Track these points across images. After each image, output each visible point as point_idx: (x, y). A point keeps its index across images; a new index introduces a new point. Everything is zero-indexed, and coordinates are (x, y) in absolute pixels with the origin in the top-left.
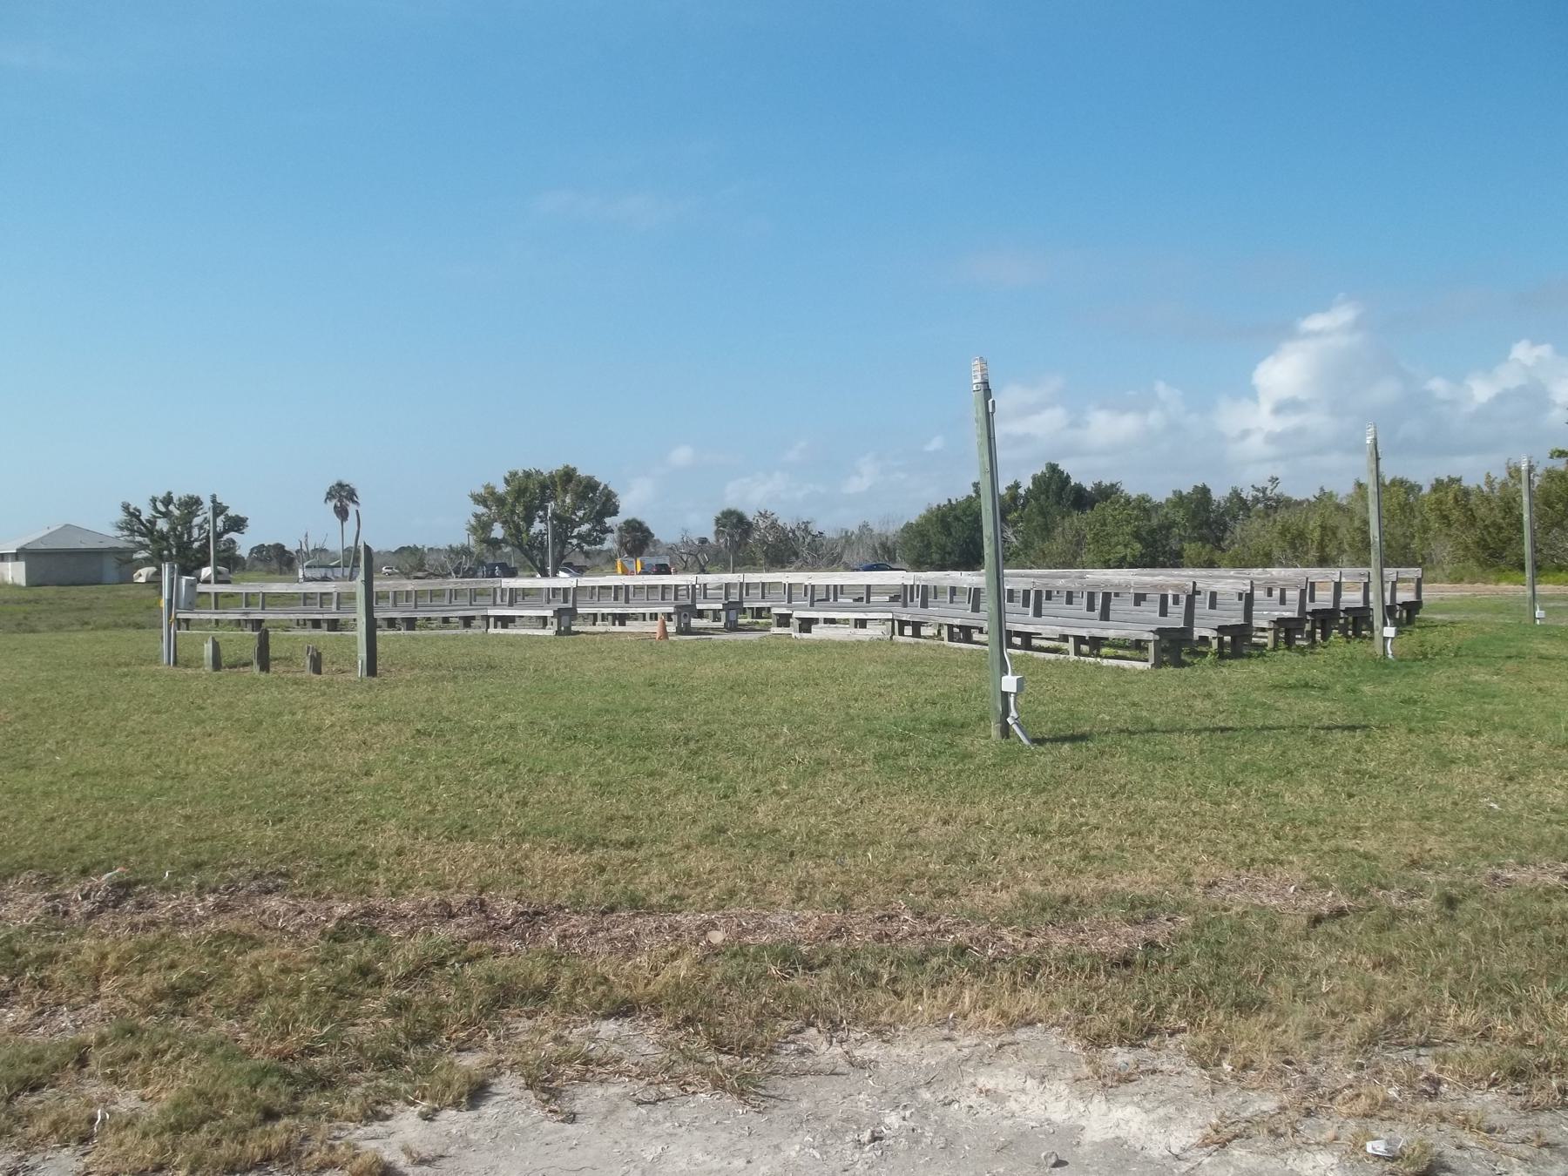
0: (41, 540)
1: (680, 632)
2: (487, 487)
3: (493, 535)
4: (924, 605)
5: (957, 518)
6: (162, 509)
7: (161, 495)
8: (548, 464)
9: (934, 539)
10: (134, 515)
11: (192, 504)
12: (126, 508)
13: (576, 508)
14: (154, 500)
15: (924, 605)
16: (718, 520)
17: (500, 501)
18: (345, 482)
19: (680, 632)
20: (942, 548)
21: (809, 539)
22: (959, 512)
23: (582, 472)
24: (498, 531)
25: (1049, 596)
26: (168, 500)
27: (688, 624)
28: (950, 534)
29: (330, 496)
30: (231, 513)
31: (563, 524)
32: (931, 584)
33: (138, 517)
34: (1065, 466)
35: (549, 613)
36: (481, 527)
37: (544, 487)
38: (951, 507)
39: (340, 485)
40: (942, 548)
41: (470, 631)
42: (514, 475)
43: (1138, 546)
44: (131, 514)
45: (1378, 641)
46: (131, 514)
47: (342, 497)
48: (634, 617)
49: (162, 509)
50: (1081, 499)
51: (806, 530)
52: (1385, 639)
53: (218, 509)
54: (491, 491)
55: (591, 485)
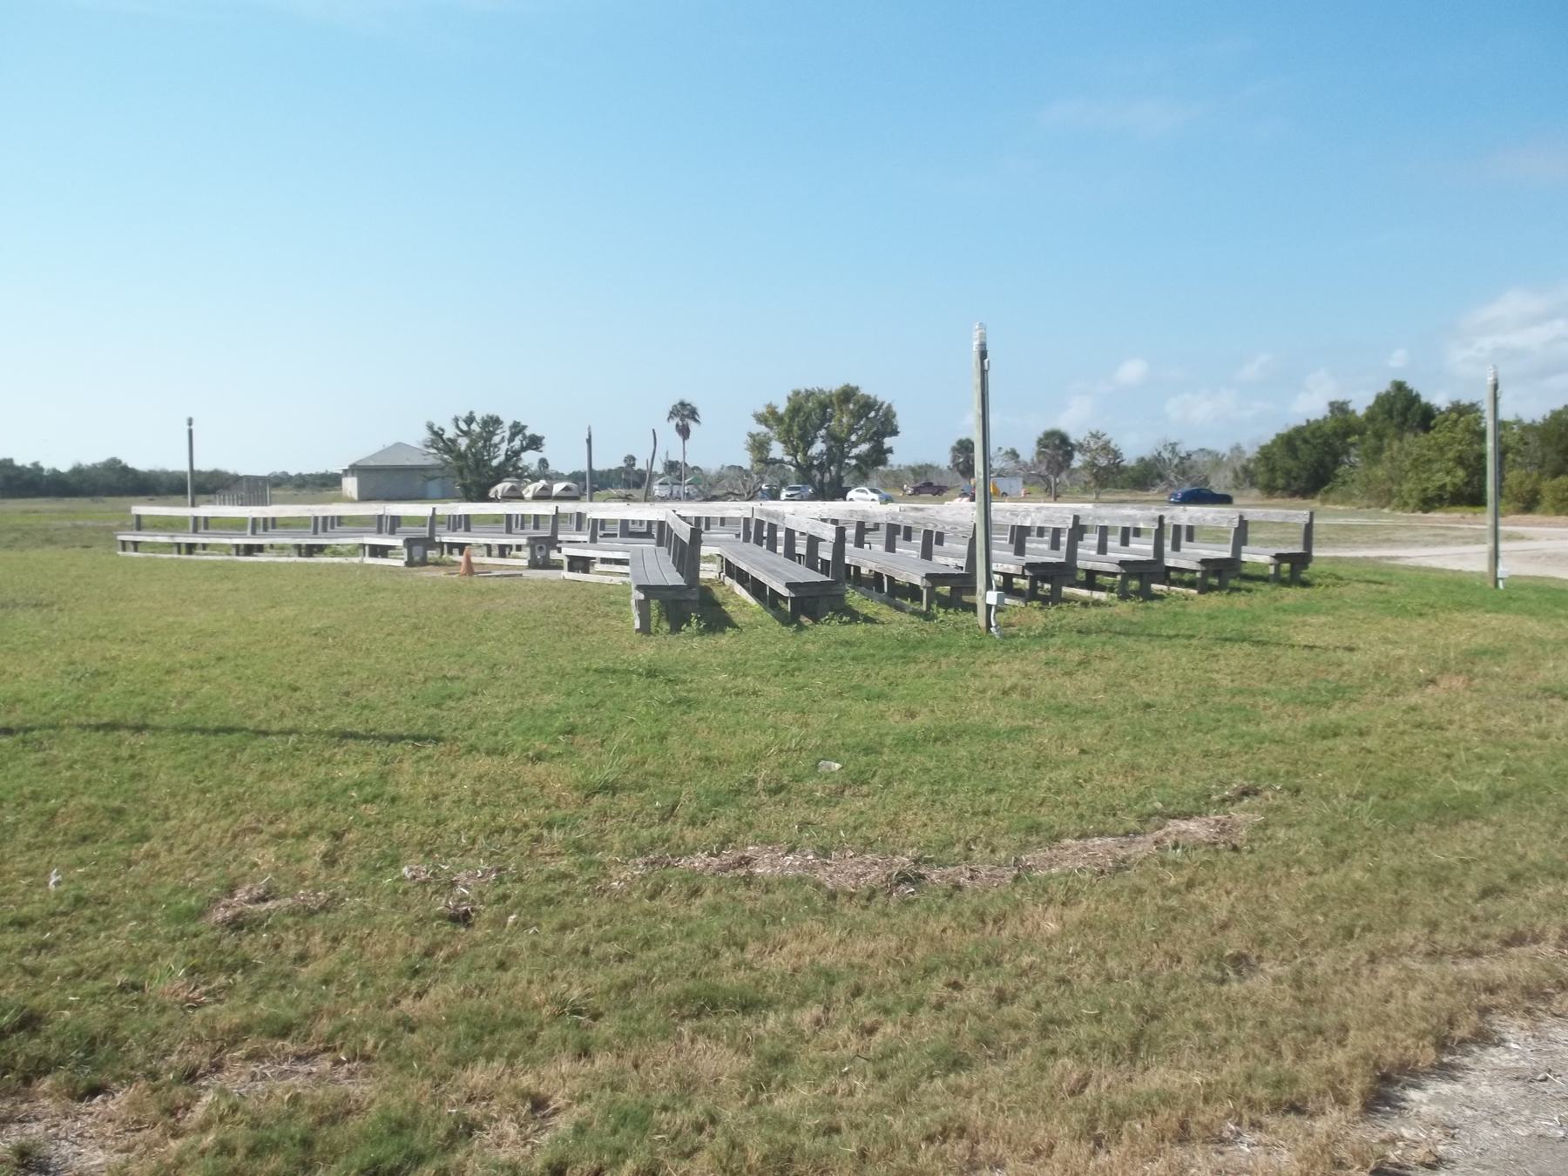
0: (371, 457)
1: (534, 565)
2: (769, 406)
3: (772, 455)
4: (890, 547)
5: (1306, 441)
6: (465, 428)
7: (464, 414)
8: (831, 383)
9: (1279, 464)
10: (437, 434)
11: (492, 423)
12: (430, 427)
13: (851, 430)
14: (456, 420)
15: (890, 547)
16: (1040, 442)
17: (779, 419)
18: (687, 401)
19: (534, 565)
20: (1288, 473)
21: (1176, 461)
22: (1307, 434)
23: (866, 390)
24: (777, 450)
25: (940, 539)
26: (470, 420)
27: (424, 557)
28: (1297, 458)
29: (673, 413)
30: (528, 432)
31: (838, 445)
32: (704, 515)
33: (441, 436)
34: (1414, 385)
35: (523, 541)
36: (759, 446)
37: (823, 406)
38: (1298, 431)
39: (683, 404)
40: (1288, 473)
41: (193, 557)
42: (797, 393)
43: (1461, 473)
44: (435, 433)
45: (981, 610)
46: (435, 433)
47: (685, 415)
48: (260, 548)
49: (465, 428)
50: (1425, 418)
51: (1173, 451)
52: (989, 607)
53: (517, 429)
54: (772, 411)
55: (868, 405)
